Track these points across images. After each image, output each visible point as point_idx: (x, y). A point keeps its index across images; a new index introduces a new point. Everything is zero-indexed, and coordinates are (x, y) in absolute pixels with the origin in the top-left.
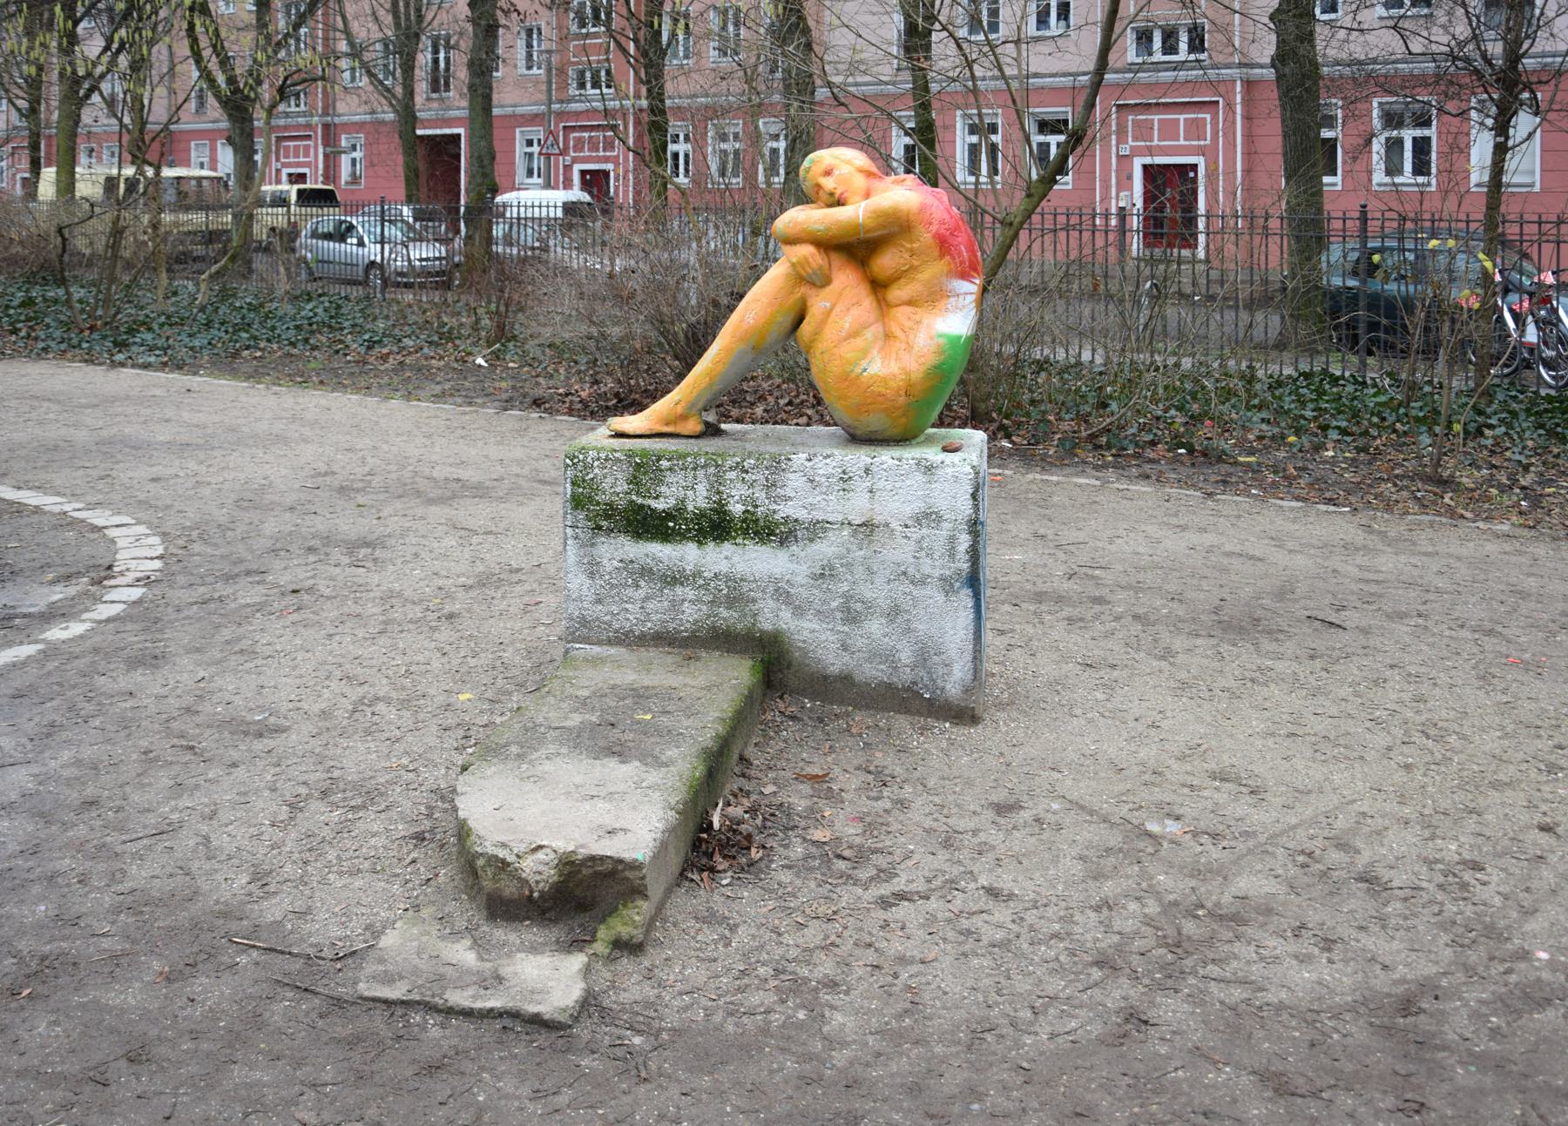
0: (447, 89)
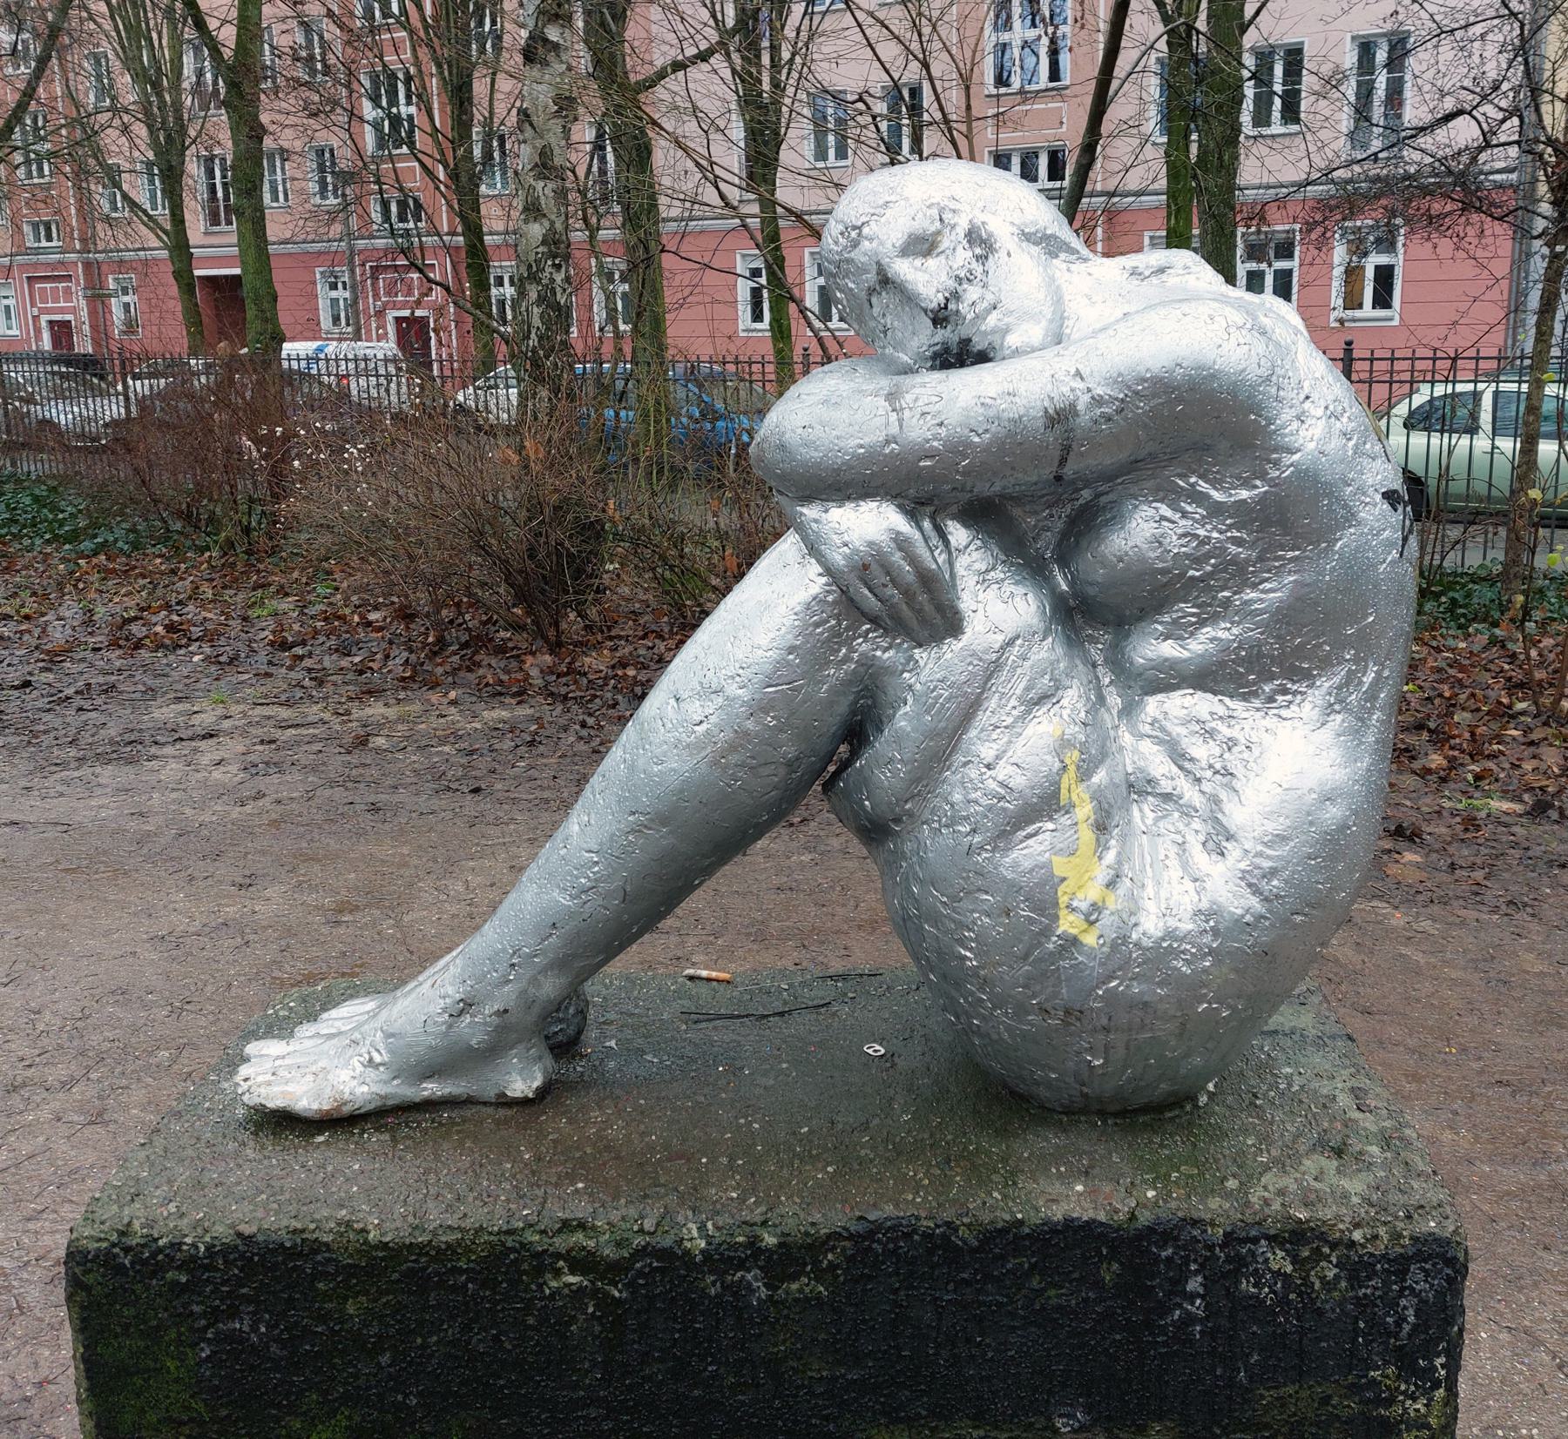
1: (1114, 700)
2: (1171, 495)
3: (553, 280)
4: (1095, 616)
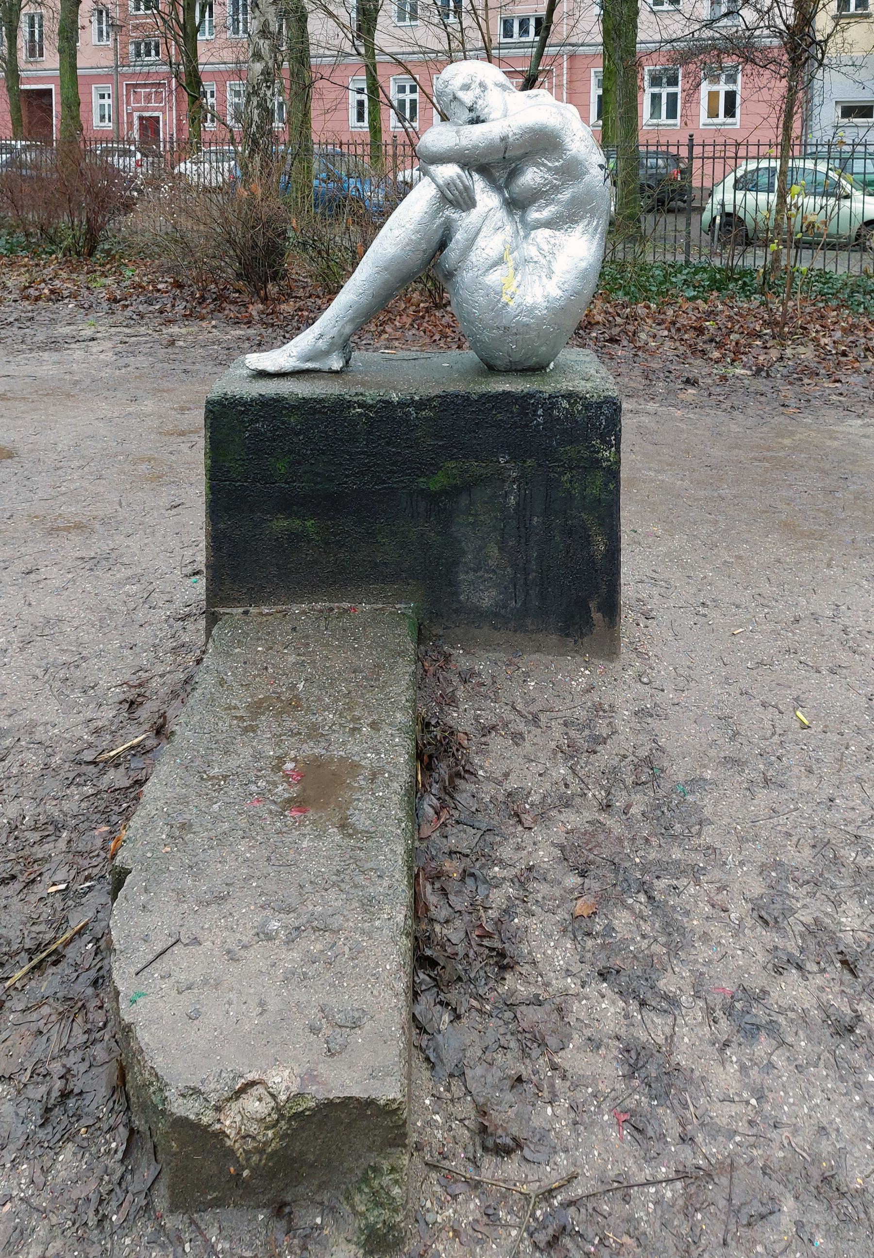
0: (41, 55)
1: (522, 233)
2: (537, 165)
3: (265, 95)
4: (516, 205)
